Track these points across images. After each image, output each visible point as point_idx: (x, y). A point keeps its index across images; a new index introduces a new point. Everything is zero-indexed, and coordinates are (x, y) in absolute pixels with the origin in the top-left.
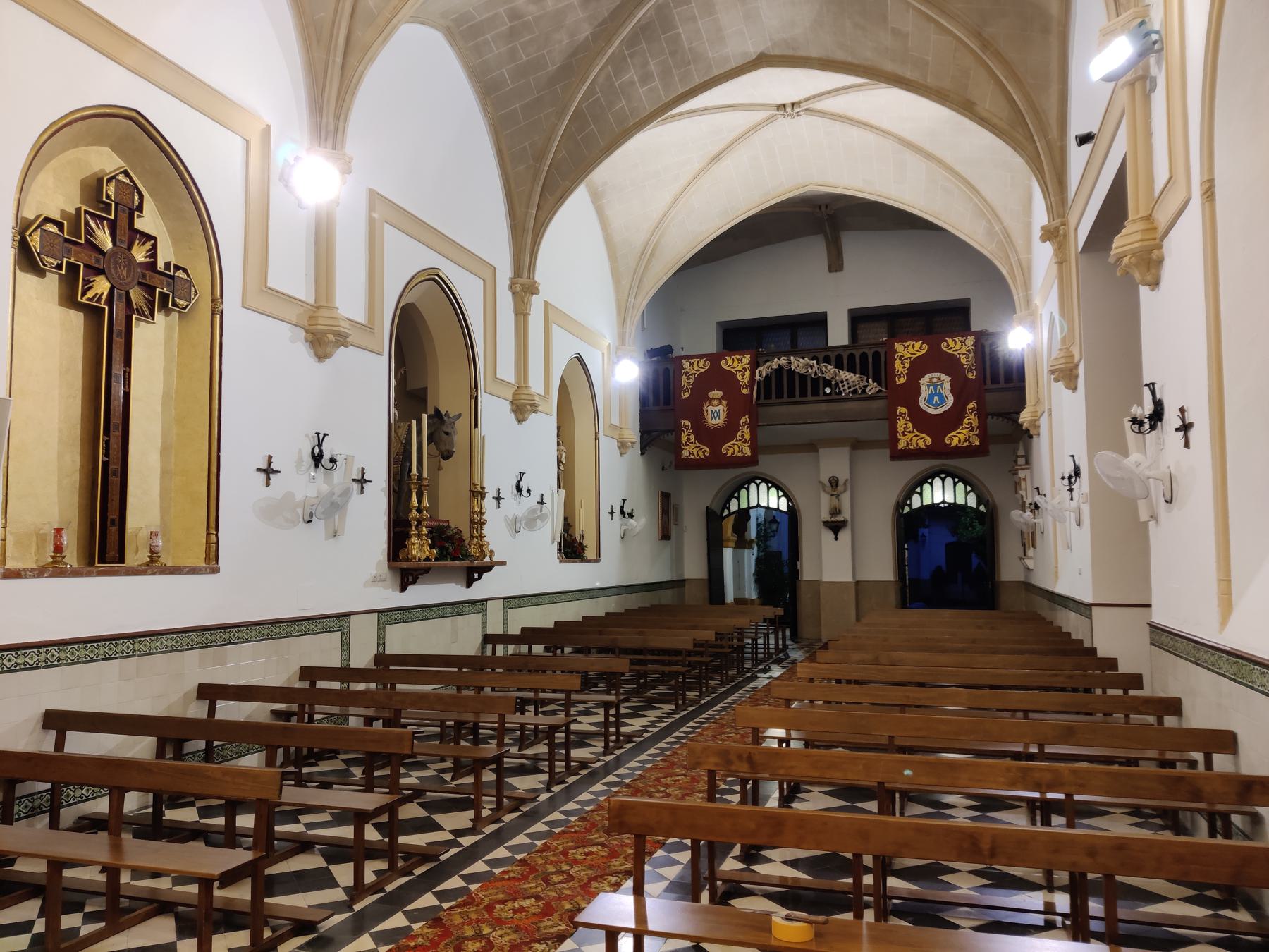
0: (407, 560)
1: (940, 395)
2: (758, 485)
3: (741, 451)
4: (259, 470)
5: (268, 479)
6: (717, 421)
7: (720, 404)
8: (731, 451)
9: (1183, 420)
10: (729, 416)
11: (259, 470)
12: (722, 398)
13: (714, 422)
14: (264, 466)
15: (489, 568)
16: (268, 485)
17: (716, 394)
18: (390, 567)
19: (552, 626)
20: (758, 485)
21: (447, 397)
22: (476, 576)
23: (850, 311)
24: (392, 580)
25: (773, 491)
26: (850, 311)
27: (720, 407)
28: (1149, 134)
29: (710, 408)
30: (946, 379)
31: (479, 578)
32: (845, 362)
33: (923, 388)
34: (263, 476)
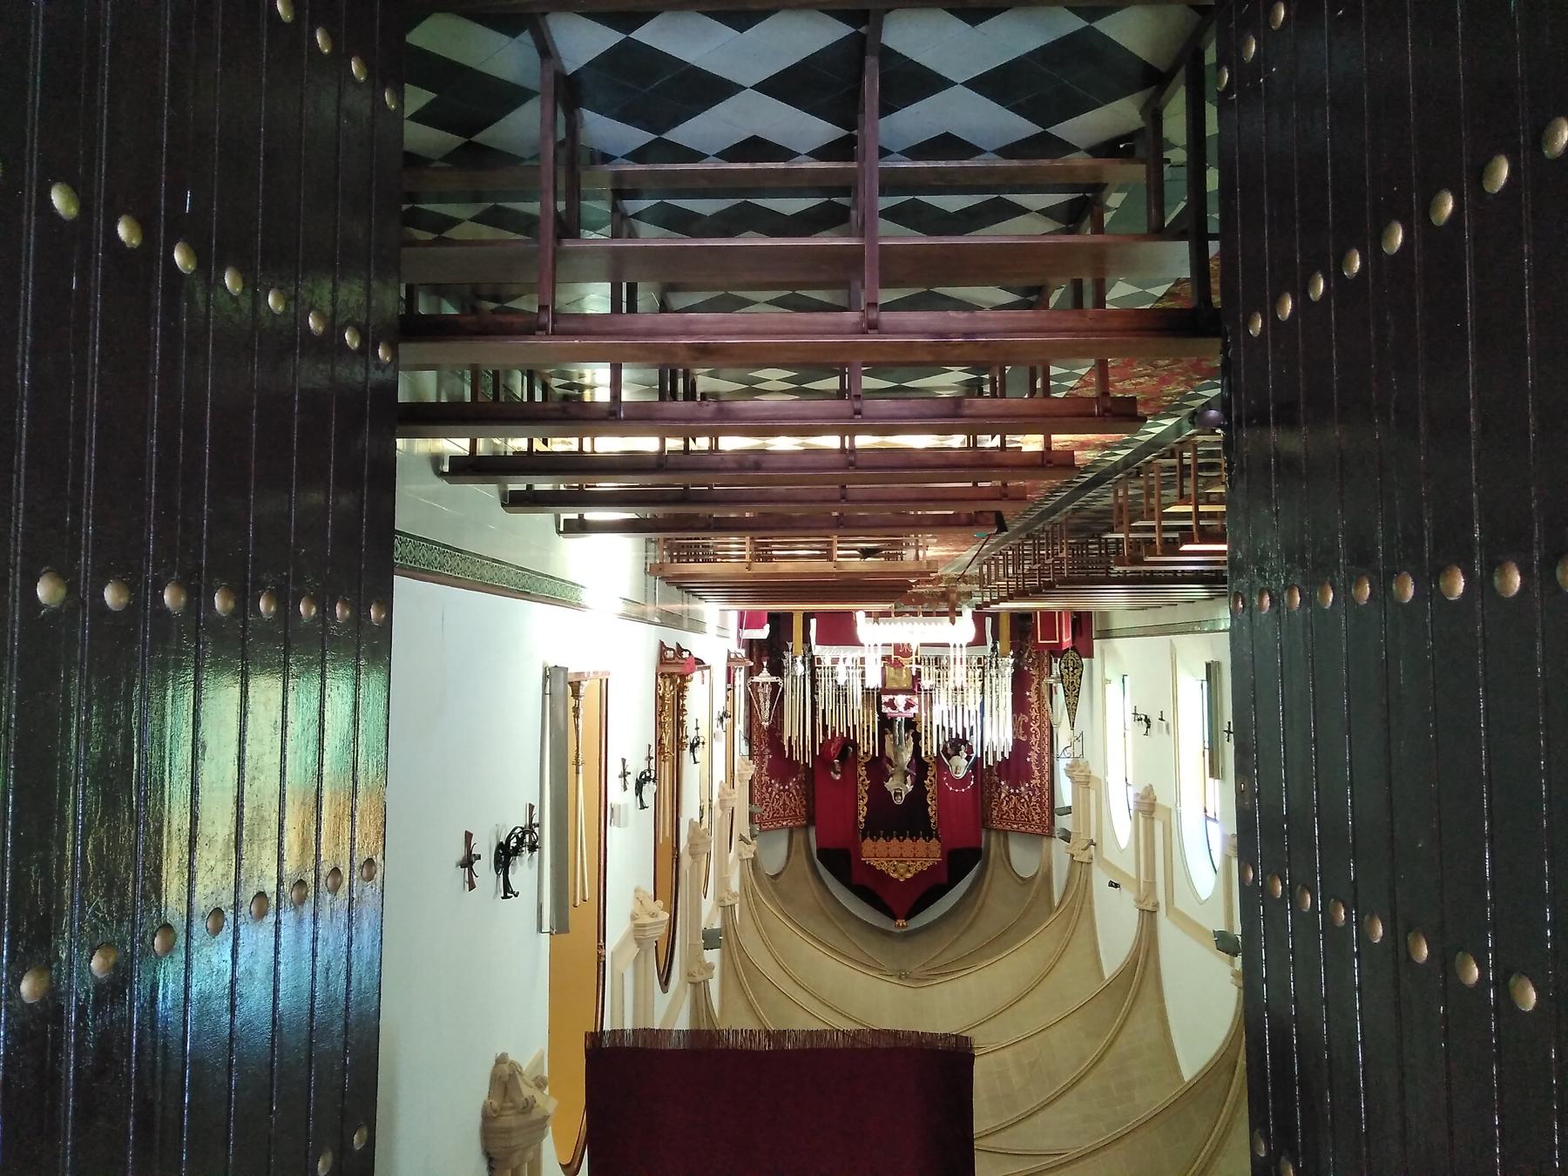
9: (471, 870)
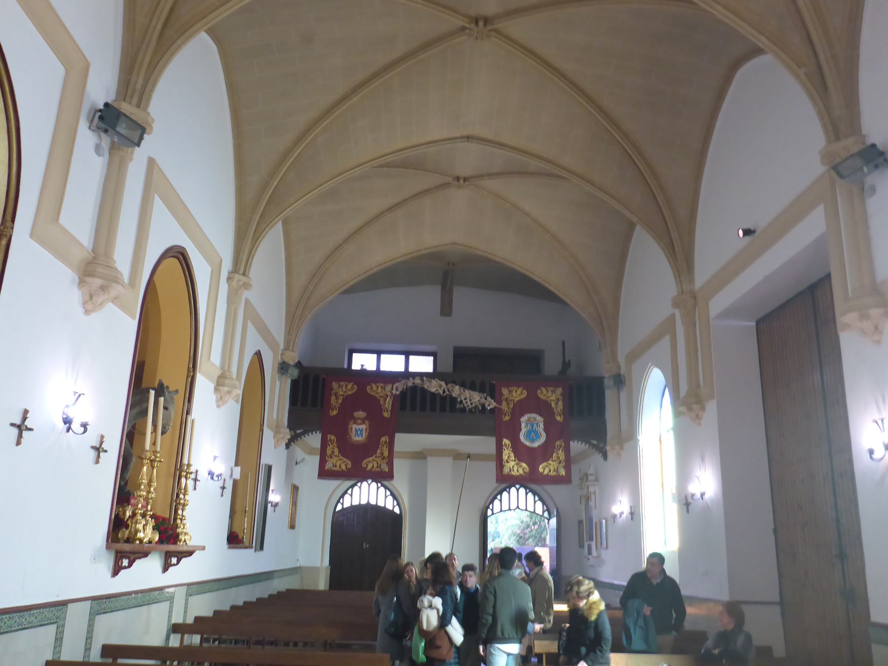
0: (128, 541)
1: (536, 432)
2: (518, 490)
3: (379, 466)
4: (12, 425)
5: (20, 436)
6: (360, 439)
7: (363, 423)
8: (370, 466)
10: (370, 436)
11: (12, 425)
12: (366, 418)
13: (357, 438)
14: (18, 421)
15: (190, 553)
16: (18, 443)
17: (360, 414)
18: (108, 547)
19: (228, 608)
20: (518, 490)
21: (168, 371)
22: (125, 562)
23: (455, 348)
24: (106, 563)
25: (530, 495)
26: (455, 348)
27: (363, 427)
28: (230, 358)
29: (354, 426)
30: (539, 419)
31: (130, 565)
32: (488, 389)
33: (523, 425)
34: (15, 431)
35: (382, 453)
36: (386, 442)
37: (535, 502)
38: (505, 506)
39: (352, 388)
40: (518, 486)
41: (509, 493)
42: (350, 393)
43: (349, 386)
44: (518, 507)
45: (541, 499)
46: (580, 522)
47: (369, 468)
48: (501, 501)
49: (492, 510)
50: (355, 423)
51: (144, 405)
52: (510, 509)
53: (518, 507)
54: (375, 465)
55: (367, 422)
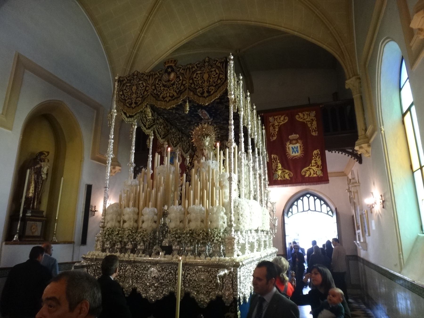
2: (308, 198)
13: (294, 154)
20: (308, 198)
25: (318, 201)
27: (298, 145)
29: (291, 146)
35: (316, 163)
36: (317, 154)
37: (321, 205)
38: (301, 209)
39: (284, 119)
40: (308, 196)
41: (302, 200)
42: (283, 123)
43: (282, 119)
44: (309, 209)
45: (326, 203)
46: (353, 216)
47: (307, 176)
48: (297, 206)
49: (292, 212)
50: (291, 143)
51: (25, 206)
52: (304, 211)
53: (309, 209)
54: (312, 173)
55: (299, 141)
